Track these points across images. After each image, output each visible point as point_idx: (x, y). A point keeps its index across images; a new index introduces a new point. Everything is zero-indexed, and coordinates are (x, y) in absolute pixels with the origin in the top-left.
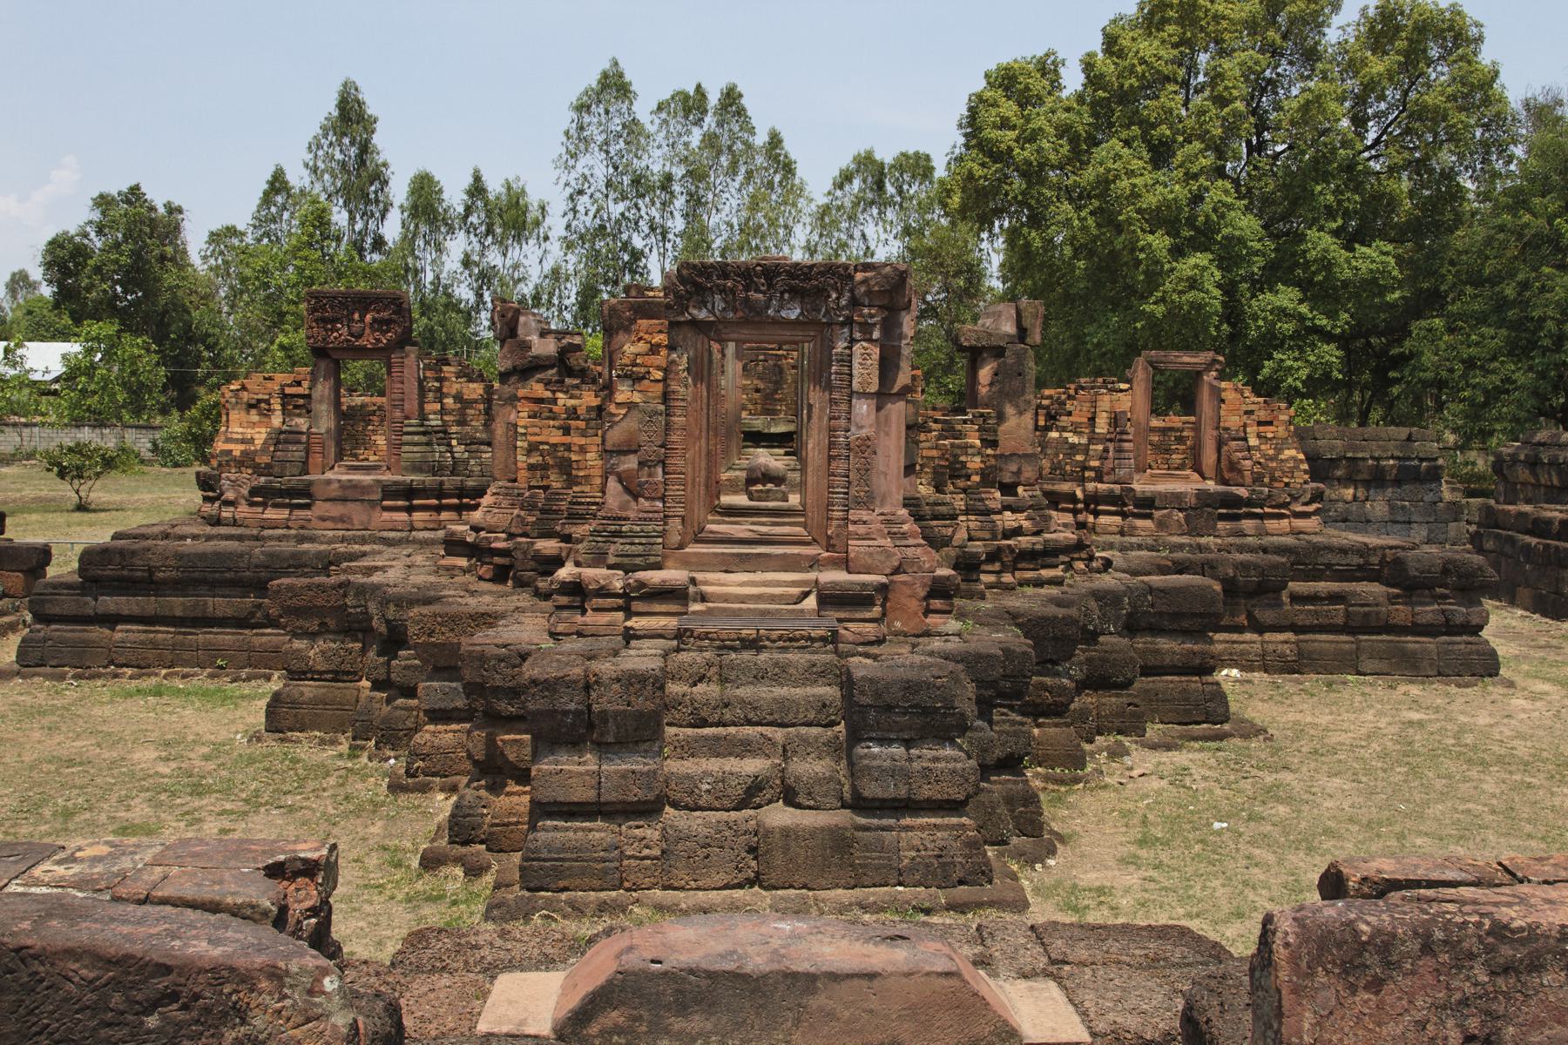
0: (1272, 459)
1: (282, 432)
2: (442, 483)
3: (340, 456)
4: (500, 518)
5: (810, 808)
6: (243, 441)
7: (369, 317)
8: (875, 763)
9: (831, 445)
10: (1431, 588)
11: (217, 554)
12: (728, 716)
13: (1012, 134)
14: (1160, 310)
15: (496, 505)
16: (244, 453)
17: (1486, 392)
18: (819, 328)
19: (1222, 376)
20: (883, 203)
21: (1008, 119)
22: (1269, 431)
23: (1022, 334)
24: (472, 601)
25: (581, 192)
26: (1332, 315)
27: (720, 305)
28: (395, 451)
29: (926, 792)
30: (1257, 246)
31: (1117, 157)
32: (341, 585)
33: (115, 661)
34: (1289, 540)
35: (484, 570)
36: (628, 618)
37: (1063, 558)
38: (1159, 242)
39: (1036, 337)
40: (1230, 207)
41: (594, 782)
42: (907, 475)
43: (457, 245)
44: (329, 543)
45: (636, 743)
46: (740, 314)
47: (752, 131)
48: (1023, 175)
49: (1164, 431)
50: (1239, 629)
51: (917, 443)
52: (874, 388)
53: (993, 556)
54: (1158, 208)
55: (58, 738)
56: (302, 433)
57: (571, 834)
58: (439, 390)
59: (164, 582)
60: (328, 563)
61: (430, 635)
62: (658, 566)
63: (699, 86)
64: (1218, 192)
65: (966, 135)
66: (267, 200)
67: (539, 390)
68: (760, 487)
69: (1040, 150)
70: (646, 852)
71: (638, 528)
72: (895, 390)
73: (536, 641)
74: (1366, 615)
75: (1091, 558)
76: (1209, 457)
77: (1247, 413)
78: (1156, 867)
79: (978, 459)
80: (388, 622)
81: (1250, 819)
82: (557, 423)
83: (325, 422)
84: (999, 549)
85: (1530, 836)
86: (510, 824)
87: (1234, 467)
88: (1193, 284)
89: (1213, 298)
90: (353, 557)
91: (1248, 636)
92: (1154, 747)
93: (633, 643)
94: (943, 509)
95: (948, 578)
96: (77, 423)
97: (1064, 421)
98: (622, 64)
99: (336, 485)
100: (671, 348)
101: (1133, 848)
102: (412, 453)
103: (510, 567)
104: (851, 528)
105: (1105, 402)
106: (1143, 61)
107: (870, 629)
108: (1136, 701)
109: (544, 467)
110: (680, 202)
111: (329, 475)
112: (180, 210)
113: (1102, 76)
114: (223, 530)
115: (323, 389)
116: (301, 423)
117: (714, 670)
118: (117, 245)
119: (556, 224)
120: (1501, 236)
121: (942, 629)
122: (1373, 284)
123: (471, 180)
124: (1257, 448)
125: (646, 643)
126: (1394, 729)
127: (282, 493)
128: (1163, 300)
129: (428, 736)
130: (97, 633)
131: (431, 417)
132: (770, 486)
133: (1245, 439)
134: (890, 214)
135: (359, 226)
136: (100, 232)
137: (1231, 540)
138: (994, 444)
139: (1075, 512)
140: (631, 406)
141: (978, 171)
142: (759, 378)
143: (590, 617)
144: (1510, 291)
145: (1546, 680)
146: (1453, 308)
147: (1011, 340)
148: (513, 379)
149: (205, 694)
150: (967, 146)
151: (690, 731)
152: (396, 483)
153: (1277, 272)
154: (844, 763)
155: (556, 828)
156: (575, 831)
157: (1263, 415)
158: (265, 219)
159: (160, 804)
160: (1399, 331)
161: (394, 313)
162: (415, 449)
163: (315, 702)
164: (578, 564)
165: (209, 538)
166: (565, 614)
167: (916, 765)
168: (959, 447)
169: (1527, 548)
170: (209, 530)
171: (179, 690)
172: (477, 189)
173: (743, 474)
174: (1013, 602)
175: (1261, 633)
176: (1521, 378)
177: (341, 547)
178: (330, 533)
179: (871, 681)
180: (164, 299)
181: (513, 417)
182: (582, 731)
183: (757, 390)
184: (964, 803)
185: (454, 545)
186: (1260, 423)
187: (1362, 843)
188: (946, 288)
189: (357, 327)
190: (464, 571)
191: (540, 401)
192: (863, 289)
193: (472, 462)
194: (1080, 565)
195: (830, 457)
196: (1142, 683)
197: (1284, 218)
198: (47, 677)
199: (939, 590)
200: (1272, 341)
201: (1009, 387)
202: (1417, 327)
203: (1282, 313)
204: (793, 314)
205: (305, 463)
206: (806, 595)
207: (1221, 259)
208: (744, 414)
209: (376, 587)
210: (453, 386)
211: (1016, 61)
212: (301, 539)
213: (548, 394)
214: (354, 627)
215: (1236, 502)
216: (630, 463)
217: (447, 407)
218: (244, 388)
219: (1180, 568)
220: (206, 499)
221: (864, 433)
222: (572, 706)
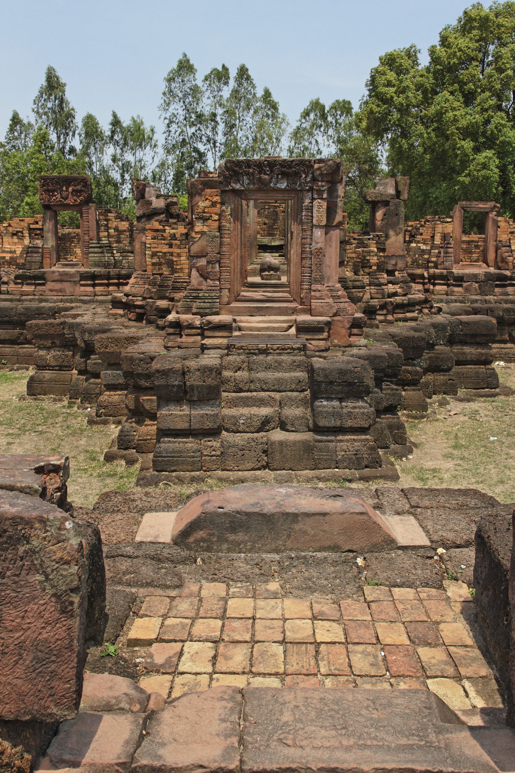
1: (29, 247)
2: (109, 272)
3: (58, 259)
4: (139, 290)
5: (293, 431)
6: (10, 252)
7: (70, 189)
8: (326, 409)
9: (303, 252)
12: (252, 387)
13: (393, 89)
14: (467, 180)
15: (136, 283)
16: (11, 258)
19: (499, 214)
21: (391, 81)
23: (398, 193)
24: (126, 331)
27: (246, 181)
28: (86, 256)
29: (349, 423)
31: (447, 100)
32: (61, 324)
35: (132, 316)
36: (203, 339)
37: (417, 307)
38: (468, 145)
40: (504, 126)
41: (188, 419)
43: (110, 150)
45: (208, 400)
46: (256, 186)
47: (254, 87)
48: (399, 110)
49: (469, 242)
52: (324, 223)
53: (383, 307)
56: (39, 248)
58: (107, 225)
60: (54, 312)
62: (217, 314)
63: (223, 66)
65: (369, 90)
66: (12, 129)
67: (156, 225)
68: (267, 273)
70: (213, 453)
72: (335, 224)
73: (158, 351)
75: (432, 307)
76: (491, 256)
78: (462, 459)
80: (85, 341)
83: (51, 243)
84: (386, 303)
87: (504, 260)
88: (485, 166)
89: (495, 173)
92: (461, 400)
95: (361, 318)
98: (188, 56)
99: (57, 274)
100: (222, 203)
101: (450, 450)
102: (94, 257)
103: (144, 314)
105: (439, 228)
106: (460, 50)
108: (453, 378)
109: (160, 264)
111: (54, 269)
113: (439, 58)
115: (49, 225)
116: (39, 243)
119: (160, 138)
121: (357, 343)
125: (212, 351)
128: (469, 175)
129: (106, 397)
131: (103, 239)
132: (272, 272)
134: (331, 132)
137: (501, 297)
138: (383, 250)
139: (424, 284)
140: (203, 233)
141: (375, 109)
143: (184, 339)
147: (392, 197)
148: (143, 220)
150: (370, 96)
151: (234, 394)
152: (87, 272)
154: (309, 409)
155: (169, 442)
161: (83, 186)
162: (96, 255)
163: (50, 381)
166: (172, 337)
167: (345, 410)
168: (366, 252)
172: (116, 122)
173: (259, 267)
174: (392, 329)
177: (61, 305)
178: (55, 298)
179: (323, 369)
181: (144, 239)
182: (182, 395)
183: (265, 224)
184: (368, 429)
185: (116, 303)
189: (65, 194)
190: (122, 316)
191: (157, 231)
193: (124, 261)
194: (426, 311)
196: (456, 369)
199: (356, 324)
204: (283, 185)
205: (42, 263)
206: (290, 327)
207: (499, 153)
209: (79, 324)
211: (395, 51)
212: (41, 301)
213: (161, 227)
215: (505, 278)
216: (203, 262)
217: (111, 234)
218: (10, 225)
219: (476, 312)
221: (319, 246)
222: (176, 383)
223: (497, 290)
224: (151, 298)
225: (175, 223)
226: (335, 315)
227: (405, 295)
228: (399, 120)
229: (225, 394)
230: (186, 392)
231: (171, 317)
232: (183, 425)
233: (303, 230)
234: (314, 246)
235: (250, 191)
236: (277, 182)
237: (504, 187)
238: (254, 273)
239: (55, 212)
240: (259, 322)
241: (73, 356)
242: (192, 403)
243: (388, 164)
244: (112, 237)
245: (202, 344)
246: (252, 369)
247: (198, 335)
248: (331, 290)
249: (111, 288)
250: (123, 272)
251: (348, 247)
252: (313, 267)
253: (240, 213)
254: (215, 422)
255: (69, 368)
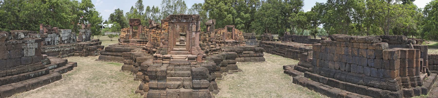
0: (241, 37)
2: (144, 40)
3: (133, 37)
4: (149, 46)
5: (187, 89)
6: (123, 36)
7: (136, 22)
8: (196, 82)
9: (190, 38)
10: (258, 52)
11: (119, 48)
12: (175, 75)
14: (226, 20)
15: (149, 44)
16: (123, 37)
17: (259, 29)
18: (188, 23)
20: (197, 9)
22: (240, 34)
23: (213, 23)
24: (145, 56)
25: (163, 8)
26: (243, 21)
27: (175, 20)
29: (203, 86)
30: (236, 14)
31: (221, 4)
32: (130, 54)
33: (108, 59)
34: (243, 47)
35: (147, 52)
36: (162, 61)
37: (218, 50)
38: (226, 13)
39: (215, 24)
40: (233, 10)
41: (157, 85)
42: (199, 41)
43: (151, 13)
44: (131, 47)
45: (163, 80)
46: (178, 21)
48: (211, 5)
49: (228, 34)
50: (238, 57)
51: (201, 37)
52: (195, 31)
53: (210, 51)
54: (226, 10)
55: (100, 69)
57: (154, 92)
58: (144, 30)
59: (113, 51)
60: (130, 50)
61: (139, 61)
62: (167, 54)
64: (232, 8)
66: (131, 9)
67: (154, 30)
68: (181, 42)
69: (213, 3)
70: (164, 95)
71: (164, 49)
72: (198, 31)
73: (151, 64)
74: (252, 55)
75: (222, 50)
76: (234, 37)
77: (238, 32)
78: (232, 93)
79: (208, 39)
80: (135, 58)
81: (242, 84)
82: (156, 34)
83: (131, 33)
84: (211, 50)
85: (273, 83)
86: (146, 88)
87: (236, 38)
88: (229, 17)
89: (232, 19)
90: (133, 49)
91: (239, 58)
92: (230, 74)
93: (163, 65)
94: (204, 45)
95: (205, 56)
96: (112, 32)
97: (217, 33)
99: (132, 41)
100: (169, 26)
101: (228, 90)
102: (141, 37)
103: (150, 52)
104: (192, 49)
105: (222, 31)
107: (195, 63)
108: (227, 68)
109: (154, 40)
110: (174, 8)
111: (131, 39)
112: (123, 11)
114: (120, 45)
115: (131, 30)
116: (129, 34)
117: (174, 69)
118: (117, 14)
119: (161, 11)
120: (260, 14)
121: (204, 62)
122: (247, 18)
123: (153, 6)
124: (239, 36)
125: (165, 65)
126: (256, 69)
127: (126, 41)
128: (226, 19)
130: (106, 56)
132: (182, 42)
133: (238, 35)
134: (198, 10)
135: (140, 12)
136: (115, 13)
137: (236, 47)
138: (210, 37)
139: (219, 44)
140: (164, 33)
141: (206, 5)
142: (182, 28)
143: (158, 61)
144: (261, 19)
145: (270, 61)
146: (255, 21)
147: (212, 24)
148: (151, 29)
149: (117, 64)
150: (205, 2)
151: (170, 77)
152: (139, 40)
153: (239, 16)
154: (191, 82)
155: (152, 91)
156: (154, 91)
157: (240, 32)
158: (131, 11)
159: (108, 79)
160: (250, 23)
163: (127, 67)
164: (157, 53)
165: (118, 46)
166: (155, 60)
167: (201, 83)
168: (206, 37)
169: (265, 46)
170: (119, 45)
171: (114, 63)
172: (153, 8)
173: (179, 40)
174: (213, 57)
175: (240, 58)
176: (262, 28)
177: (132, 48)
178: (131, 46)
179: (195, 71)
180: (121, 19)
181: (151, 34)
182: (155, 78)
183: (182, 29)
184: (208, 88)
185: (144, 49)
186: (239, 33)
187: (256, 86)
188: (203, 17)
189: (135, 23)
190: (145, 52)
192: (194, 18)
194: (220, 51)
195: (189, 40)
196: (228, 65)
197: (238, 11)
198: (101, 61)
199: (204, 57)
200: (237, 24)
201: (211, 30)
202: (252, 22)
203: (238, 21)
204: (185, 21)
205: (129, 38)
206: (186, 58)
207: (232, 15)
208: (180, 32)
209: (134, 54)
210: (145, 29)
212: (128, 47)
213: (155, 31)
214: (132, 59)
215: (237, 42)
216: (163, 40)
218: (123, 30)
219: (231, 51)
220: (119, 42)
221: (194, 37)
222: (154, 75)
223: (235, 45)
224: (152, 48)
225: (158, 30)
226: (198, 55)
227: (215, 48)
228: (211, 7)
229: (168, 77)
230: (156, 77)
231: (155, 55)
232: (156, 87)
233: (190, 33)
234: (193, 37)
235: (176, 22)
236: (183, 20)
237: (233, 22)
238: (178, 41)
239: (133, 27)
240: (178, 57)
241: (133, 61)
242: (158, 80)
243: (209, 16)
244: (145, 32)
245: (162, 63)
246: (175, 70)
247: (161, 60)
248: (197, 48)
249: (144, 44)
250: (147, 40)
251: (201, 36)
252: (192, 42)
253: (34, 81)
254: (165, 86)
255: (131, 64)
